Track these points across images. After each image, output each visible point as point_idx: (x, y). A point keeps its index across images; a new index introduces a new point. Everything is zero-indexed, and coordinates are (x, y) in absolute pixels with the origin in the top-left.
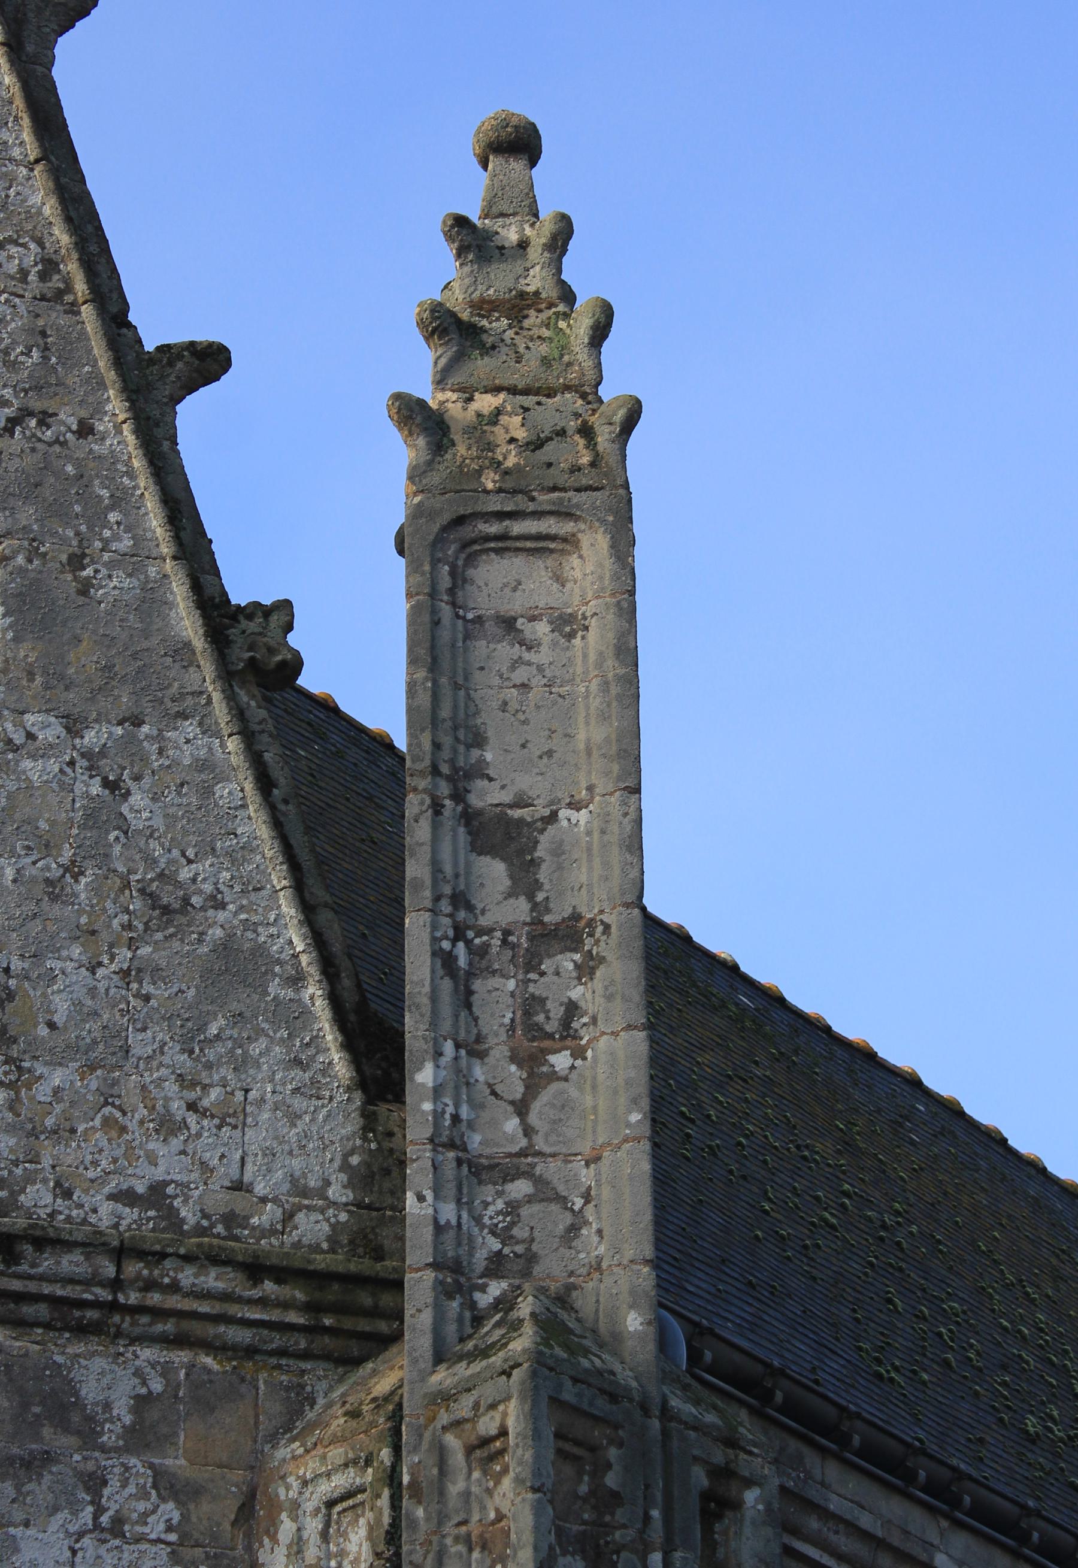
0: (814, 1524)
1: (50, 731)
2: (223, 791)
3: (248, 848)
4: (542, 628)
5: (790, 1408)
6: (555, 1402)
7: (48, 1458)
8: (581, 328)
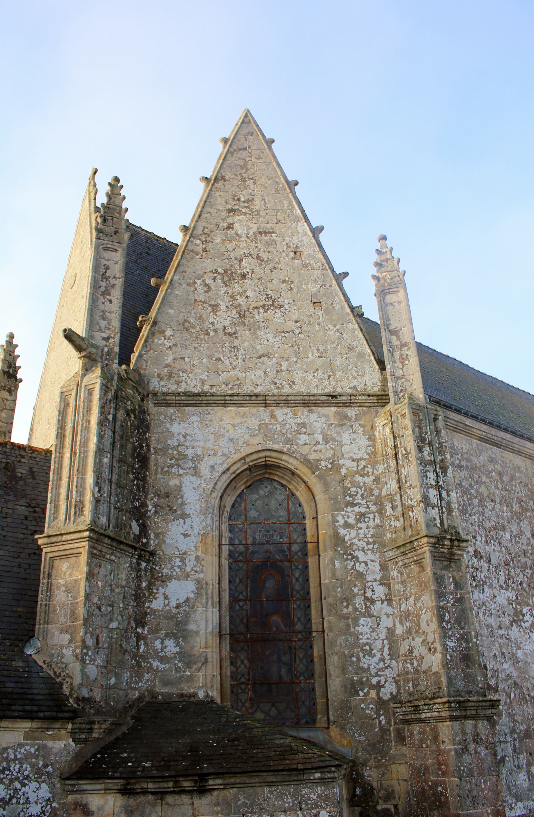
0: (449, 420)
1: (332, 327)
2: (356, 332)
4: (396, 304)
5: (444, 405)
7: (345, 424)
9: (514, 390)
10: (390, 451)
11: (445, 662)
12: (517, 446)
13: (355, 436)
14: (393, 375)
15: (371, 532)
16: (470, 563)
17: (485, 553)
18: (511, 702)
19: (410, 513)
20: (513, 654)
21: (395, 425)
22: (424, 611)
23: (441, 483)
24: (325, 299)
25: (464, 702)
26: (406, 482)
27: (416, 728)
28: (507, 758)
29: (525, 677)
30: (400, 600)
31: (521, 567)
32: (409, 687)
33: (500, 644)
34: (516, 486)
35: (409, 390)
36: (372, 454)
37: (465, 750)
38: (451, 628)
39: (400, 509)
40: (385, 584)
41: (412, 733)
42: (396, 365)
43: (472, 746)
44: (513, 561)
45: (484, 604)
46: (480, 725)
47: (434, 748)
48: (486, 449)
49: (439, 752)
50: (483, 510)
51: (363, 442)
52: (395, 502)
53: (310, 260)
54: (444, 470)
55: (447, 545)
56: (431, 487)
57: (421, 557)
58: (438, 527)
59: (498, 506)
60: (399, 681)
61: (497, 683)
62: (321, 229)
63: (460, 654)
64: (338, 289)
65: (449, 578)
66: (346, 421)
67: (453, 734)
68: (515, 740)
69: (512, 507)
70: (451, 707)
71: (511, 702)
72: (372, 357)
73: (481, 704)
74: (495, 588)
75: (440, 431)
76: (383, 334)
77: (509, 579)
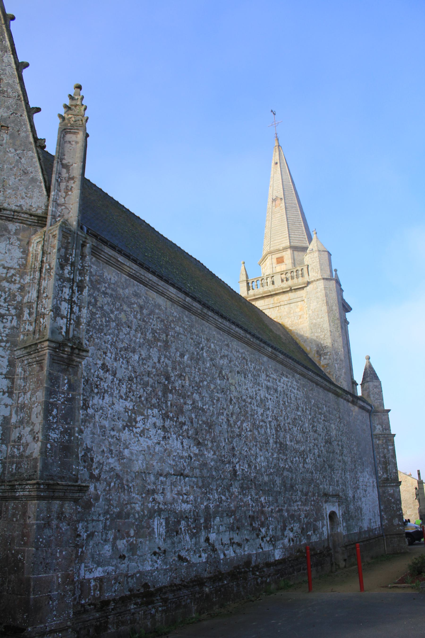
0: (103, 253)
1: (13, 150)
2: (34, 160)
3: (36, 167)
4: (74, 143)
5: (100, 239)
6: (62, 231)
7: (4, 235)
8: (83, 108)
9: (187, 256)
10: (38, 265)
11: (44, 450)
12: (161, 288)
13: (11, 247)
14: (55, 201)
15: (7, 332)
16: (96, 373)
17: (112, 368)
18: (110, 490)
19: (41, 320)
20: (120, 452)
21: (46, 243)
22: (36, 405)
23: (75, 299)
24: (13, 125)
25: (53, 485)
26: (44, 292)
27: (12, 504)
28: (96, 533)
29: (127, 471)
30: (19, 393)
31: (143, 384)
32: (13, 469)
33: (109, 442)
34: (153, 320)
35: (66, 217)
36: (22, 265)
37: (48, 525)
38: (56, 422)
39: (34, 315)
40: (9, 378)
41: (7, 509)
42: (60, 194)
43: (54, 523)
44: (136, 378)
45: (102, 408)
46: (67, 505)
47: (22, 522)
48: (134, 285)
49: (25, 525)
50: (119, 332)
51: (17, 253)
52: (33, 309)
53: (8, 89)
54: (81, 289)
55: (67, 352)
56: (64, 301)
57: (42, 358)
58: (63, 336)
59: (133, 332)
60: (6, 463)
61: (100, 473)
62: (26, 65)
63: (61, 445)
64: (28, 120)
65: (64, 380)
66: (4, 233)
67: (38, 511)
68: (107, 519)
69: (146, 335)
70: (39, 488)
71: (110, 490)
72: (43, 184)
73: (69, 488)
74: (116, 397)
75: (86, 256)
76: (55, 164)
77: (130, 392)
